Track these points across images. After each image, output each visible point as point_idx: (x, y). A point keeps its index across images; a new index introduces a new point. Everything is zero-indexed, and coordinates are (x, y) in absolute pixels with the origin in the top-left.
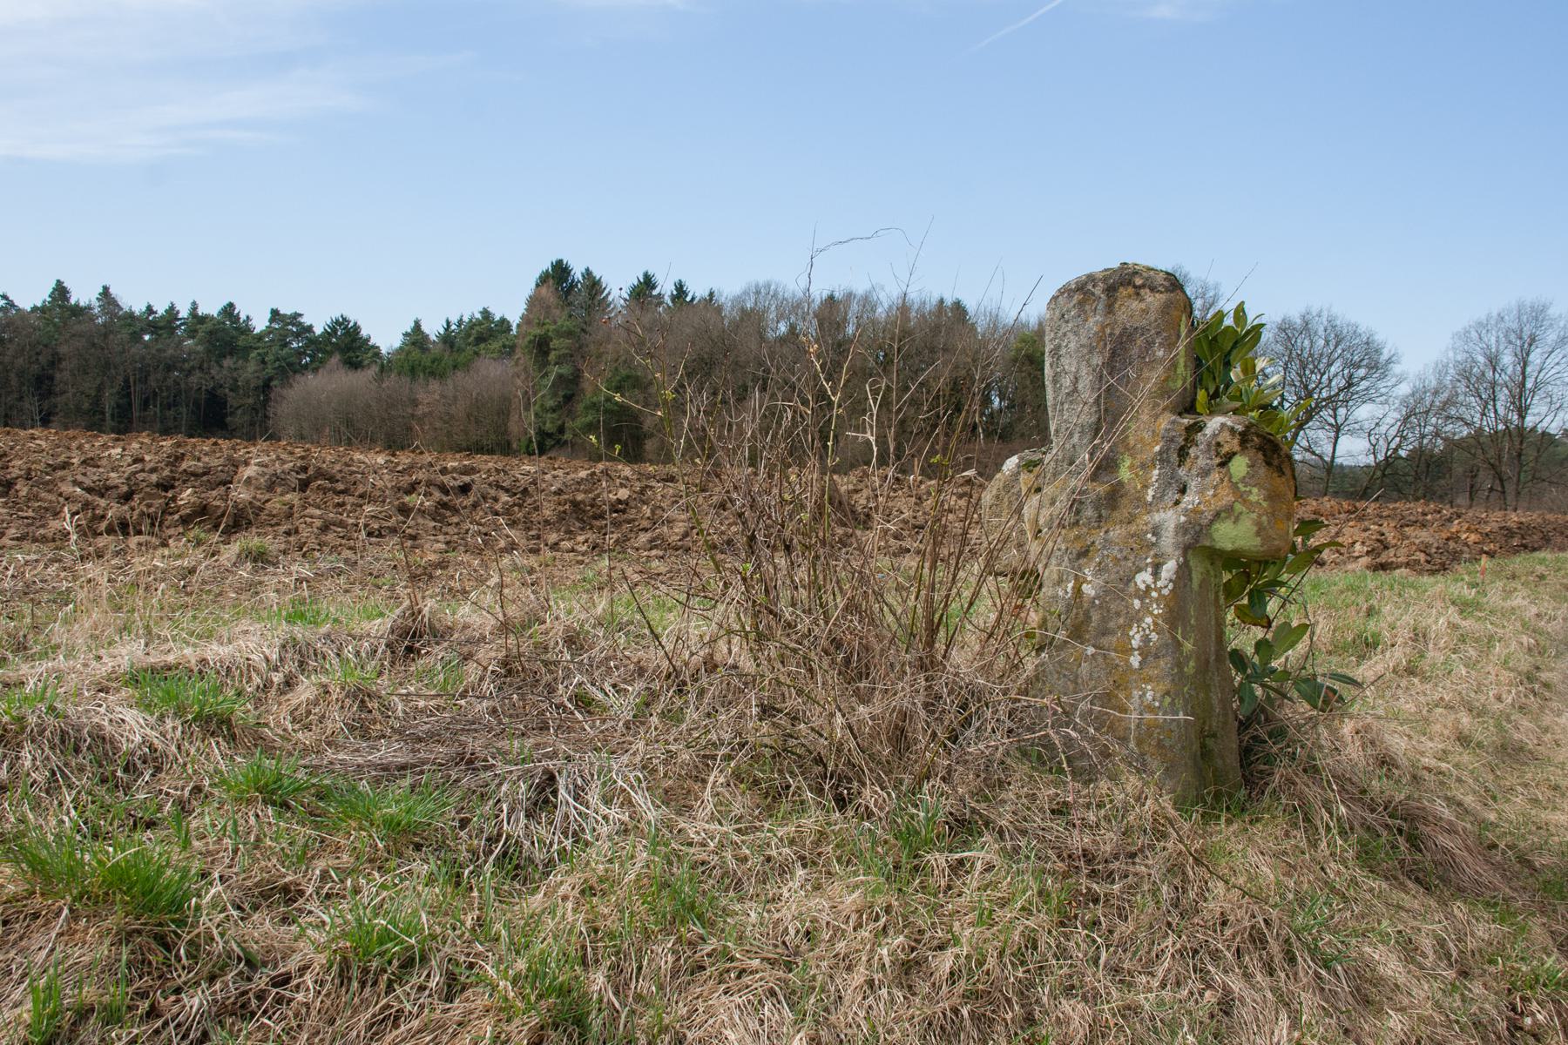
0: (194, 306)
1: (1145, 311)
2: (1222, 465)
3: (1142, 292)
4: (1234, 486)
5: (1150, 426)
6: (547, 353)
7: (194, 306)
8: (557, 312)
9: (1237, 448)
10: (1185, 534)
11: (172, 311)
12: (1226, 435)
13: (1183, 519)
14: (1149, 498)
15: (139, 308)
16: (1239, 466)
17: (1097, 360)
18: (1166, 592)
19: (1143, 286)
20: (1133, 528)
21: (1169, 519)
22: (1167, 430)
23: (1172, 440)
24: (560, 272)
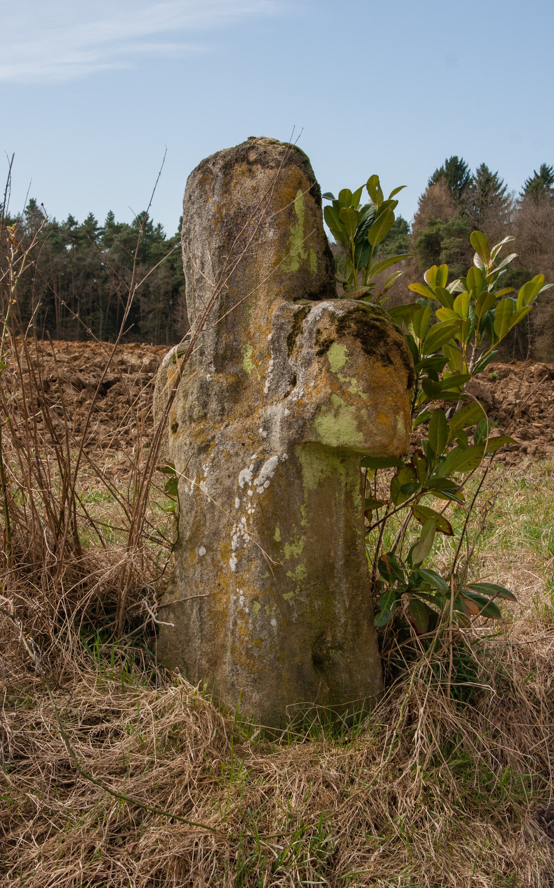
0: (111, 216)
1: (255, 189)
2: (321, 353)
3: (254, 168)
4: (332, 377)
5: (266, 312)
6: (437, 253)
7: (111, 216)
8: (448, 211)
9: (334, 336)
10: (290, 428)
11: (91, 221)
12: (326, 321)
13: (287, 412)
14: (266, 390)
15: (61, 219)
16: (338, 354)
17: (216, 243)
18: (260, 490)
19: (256, 162)
20: (249, 422)
21: (278, 411)
22: (277, 317)
23: (281, 328)
24: (454, 170)
